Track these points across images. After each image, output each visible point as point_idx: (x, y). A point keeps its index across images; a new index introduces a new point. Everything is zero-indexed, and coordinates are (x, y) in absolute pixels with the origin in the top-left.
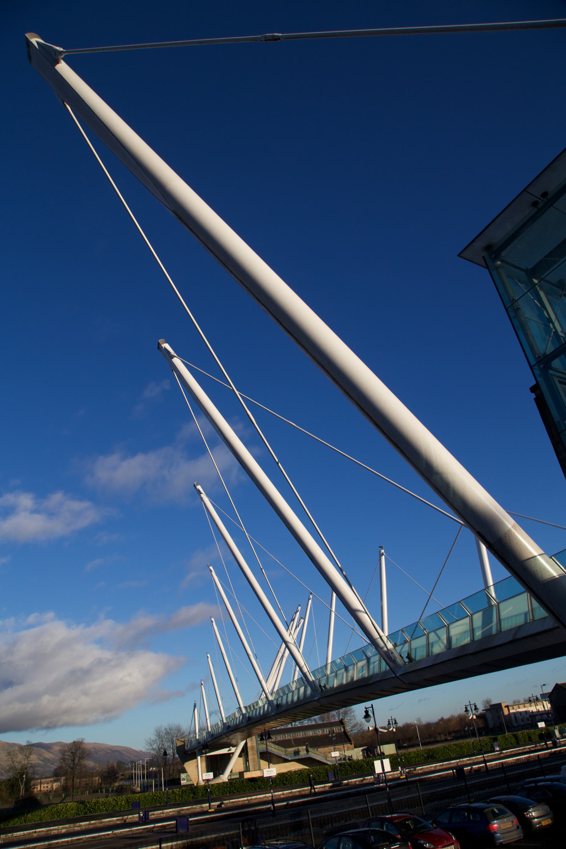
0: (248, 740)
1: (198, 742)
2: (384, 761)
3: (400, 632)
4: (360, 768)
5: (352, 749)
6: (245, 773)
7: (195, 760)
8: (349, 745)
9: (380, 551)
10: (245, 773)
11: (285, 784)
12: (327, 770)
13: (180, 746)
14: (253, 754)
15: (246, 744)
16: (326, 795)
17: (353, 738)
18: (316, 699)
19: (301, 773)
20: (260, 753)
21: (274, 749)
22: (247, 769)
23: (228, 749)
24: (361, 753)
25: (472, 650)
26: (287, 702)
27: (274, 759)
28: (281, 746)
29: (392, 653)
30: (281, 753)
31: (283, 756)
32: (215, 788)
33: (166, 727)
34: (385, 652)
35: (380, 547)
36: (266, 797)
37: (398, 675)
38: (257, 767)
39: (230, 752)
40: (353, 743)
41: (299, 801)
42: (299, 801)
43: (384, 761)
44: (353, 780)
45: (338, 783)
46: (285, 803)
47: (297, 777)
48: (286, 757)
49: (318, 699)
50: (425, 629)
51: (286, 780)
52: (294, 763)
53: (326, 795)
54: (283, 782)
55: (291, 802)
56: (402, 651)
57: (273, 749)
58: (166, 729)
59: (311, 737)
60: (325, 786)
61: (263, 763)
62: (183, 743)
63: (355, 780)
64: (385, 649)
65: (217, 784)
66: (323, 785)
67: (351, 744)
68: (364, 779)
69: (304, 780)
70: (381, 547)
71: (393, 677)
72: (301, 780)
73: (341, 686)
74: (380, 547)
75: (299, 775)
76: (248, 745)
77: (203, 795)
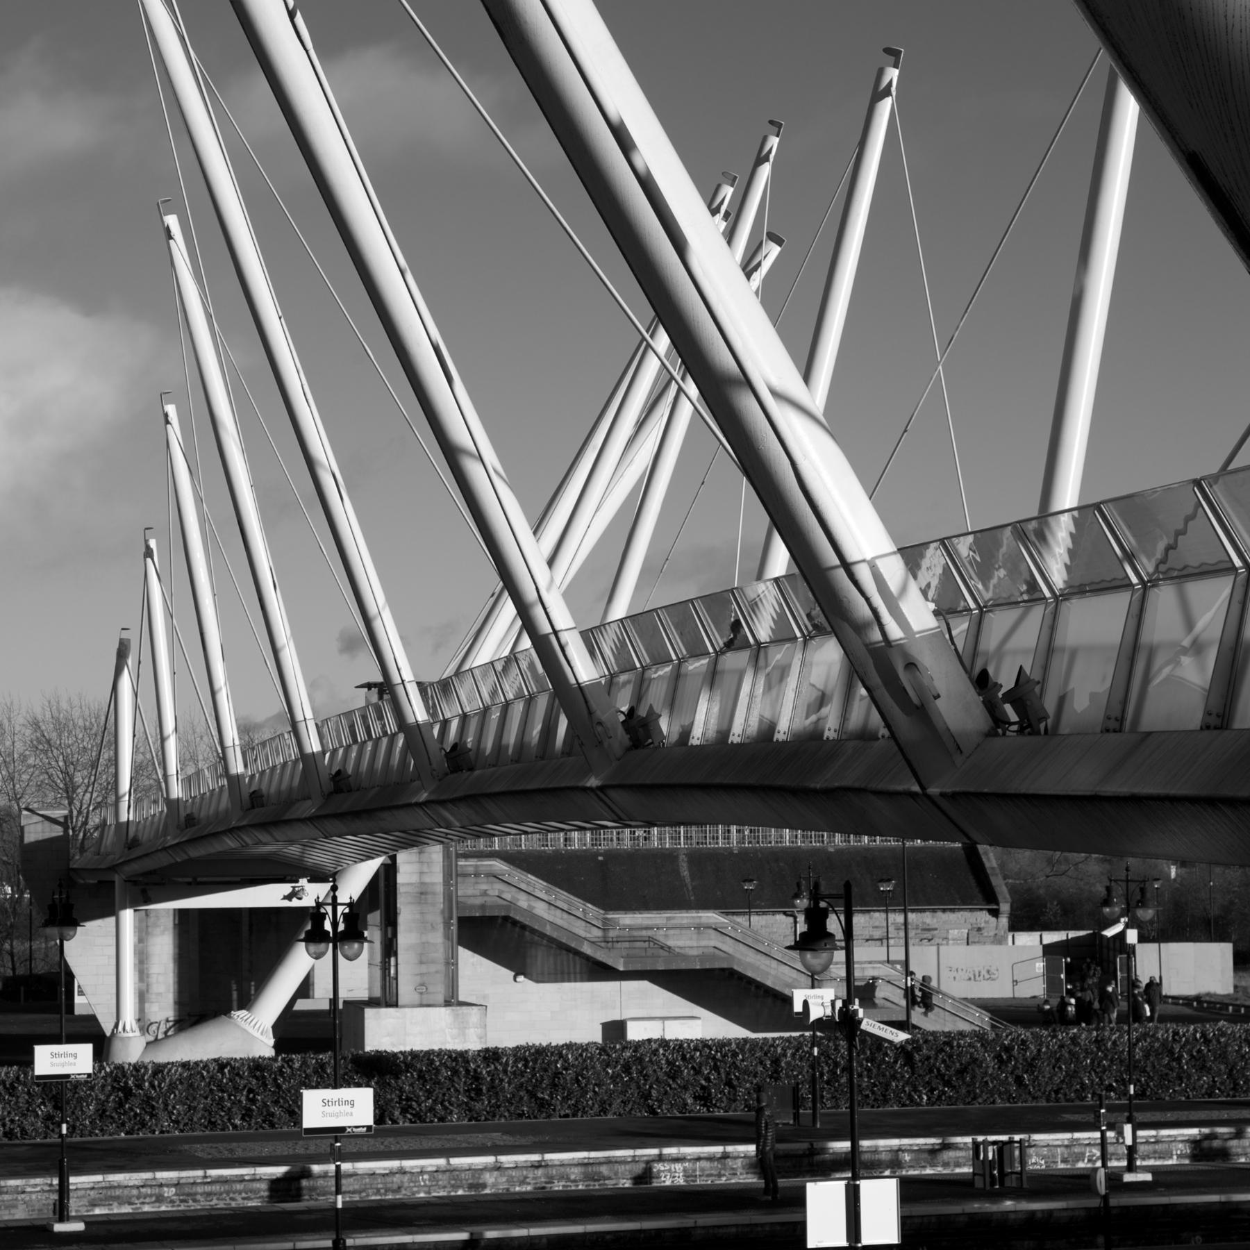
0: (403, 858)
1: (129, 840)
2: (867, 1187)
3: (1008, 532)
4: (961, 1072)
5: (998, 940)
6: (369, 1013)
7: (112, 920)
8: (983, 917)
9: (881, 73)
10: (369, 1013)
11: (542, 1105)
12: (776, 1062)
13: (38, 844)
14: (424, 926)
15: (388, 873)
16: (687, 1221)
17: (1013, 890)
18: (593, 782)
19: (640, 1060)
20: (462, 920)
21: (543, 905)
22: (387, 998)
23: (286, 888)
24: (1040, 966)
25: (505, 1198)
26: (499, 746)
27: (540, 958)
28: (587, 899)
29: (911, 665)
30: (579, 928)
31: (587, 949)
32: (172, 1087)
33: (38, 712)
34: (872, 650)
35: (888, 51)
36: (402, 1171)
37: (933, 790)
38: (439, 992)
39: (295, 903)
40: (1005, 907)
41: (536, 1231)
42: (536, 1231)
43: (867, 1187)
44: (883, 1143)
45: (801, 1146)
46: (464, 1236)
47: (614, 1078)
48: (601, 956)
49: (601, 788)
50: (1130, 557)
51: (554, 1085)
52: (645, 985)
53: (687, 1221)
54: (532, 1095)
55: (491, 1234)
56: (1011, 645)
57: (541, 909)
58: (36, 725)
59: (786, 851)
60: (725, 1156)
61: (475, 970)
62: (58, 831)
63: (895, 1142)
64: (876, 636)
65: (185, 1065)
66: (717, 1149)
67: (995, 913)
68: (946, 1147)
69: (647, 1096)
70: (893, 53)
71: (913, 795)
72: (632, 1092)
73: (721, 743)
74: (888, 51)
75: (627, 1069)
76: (401, 879)
77: (102, 1113)
